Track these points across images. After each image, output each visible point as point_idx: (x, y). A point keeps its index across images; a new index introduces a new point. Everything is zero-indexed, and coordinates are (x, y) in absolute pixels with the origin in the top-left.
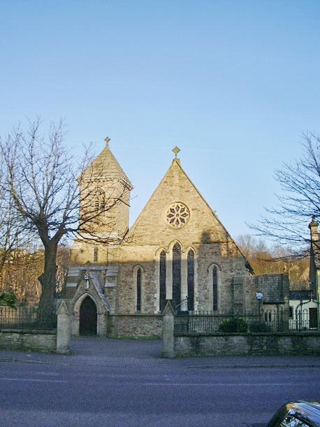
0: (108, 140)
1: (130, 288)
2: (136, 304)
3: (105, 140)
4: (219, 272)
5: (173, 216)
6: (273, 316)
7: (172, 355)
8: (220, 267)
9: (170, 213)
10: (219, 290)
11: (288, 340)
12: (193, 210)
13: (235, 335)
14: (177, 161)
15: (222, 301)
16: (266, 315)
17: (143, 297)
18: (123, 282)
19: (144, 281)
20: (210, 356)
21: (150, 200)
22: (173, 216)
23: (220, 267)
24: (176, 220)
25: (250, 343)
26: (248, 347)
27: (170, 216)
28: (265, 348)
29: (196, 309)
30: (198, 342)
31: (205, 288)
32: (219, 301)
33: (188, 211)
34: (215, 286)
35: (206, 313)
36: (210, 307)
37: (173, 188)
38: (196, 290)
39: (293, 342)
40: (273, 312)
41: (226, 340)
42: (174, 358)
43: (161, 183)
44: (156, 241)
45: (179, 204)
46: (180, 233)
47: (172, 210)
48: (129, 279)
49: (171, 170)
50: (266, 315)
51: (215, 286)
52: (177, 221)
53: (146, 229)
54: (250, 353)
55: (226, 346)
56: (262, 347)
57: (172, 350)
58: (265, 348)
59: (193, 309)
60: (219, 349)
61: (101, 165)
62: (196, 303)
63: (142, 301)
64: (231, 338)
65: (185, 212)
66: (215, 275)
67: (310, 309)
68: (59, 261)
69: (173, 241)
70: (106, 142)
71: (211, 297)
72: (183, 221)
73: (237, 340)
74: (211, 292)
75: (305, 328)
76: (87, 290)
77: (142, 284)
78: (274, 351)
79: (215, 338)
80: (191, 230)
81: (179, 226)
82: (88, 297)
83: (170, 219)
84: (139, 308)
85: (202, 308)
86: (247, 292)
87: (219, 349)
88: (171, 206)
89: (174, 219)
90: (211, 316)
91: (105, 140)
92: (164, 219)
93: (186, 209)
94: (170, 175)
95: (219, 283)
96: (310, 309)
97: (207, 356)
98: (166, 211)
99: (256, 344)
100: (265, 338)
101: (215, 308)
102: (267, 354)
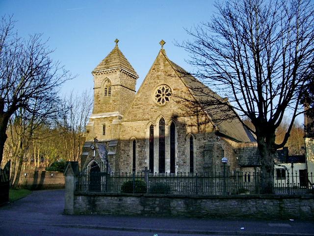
0: (117, 41)
1: (128, 156)
2: (132, 168)
3: (115, 42)
4: (194, 140)
5: (160, 96)
6: (252, 177)
7: (72, 212)
8: (195, 136)
9: (158, 93)
10: (195, 155)
11: (181, 202)
12: (174, 90)
13: (128, 196)
14: (163, 51)
15: (197, 165)
16: (245, 176)
17: (137, 163)
18: (123, 150)
19: (137, 149)
20: (105, 215)
21: (143, 84)
22: (160, 96)
23: (195, 136)
24: (162, 99)
25: (143, 204)
26: (141, 208)
27: (158, 96)
28: (157, 209)
29: (176, 171)
30: (94, 201)
31: (183, 154)
32: (195, 165)
33: (171, 91)
34: (192, 153)
35: (183, 175)
36: (188, 170)
37: (159, 73)
38: (176, 156)
39: (185, 203)
40: (251, 174)
41: (120, 200)
42: (74, 215)
43: (150, 71)
44: (146, 117)
45: (164, 86)
46: (165, 110)
47: (159, 91)
48: (127, 148)
49: (158, 60)
50: (245, 176)
51: (192, 153)
52: (163, 100)
53: (139, 108)
54: (142, 214)
55: (119, 206)
56: (154, 208)
57: (72, 207)
58: (157, 209)
59: (174, 172)
60: (113, 209)
61: (52, 60)
62: (177, 167)
63: (136, 165)
64: (124, 199)
65: (169, 92)
66: (191, 143)
67: (300, 170)
68: (293, 126)
69: (159, 116)
70: (115, 43)
71: (188, 161)
72: (167, 99)
73: (130, 201)
74: (189, 157)
75: (295, 188)
76: (94, 157)
77: (137, 152)
78: (167, 213)
79: (110, 198)
80: (172, 106)
81: (164, 104)
82: (94, 163)
83: (158, 99)
84: (134, 170)
85: (181, 171)
86: (218, 156)
87: (113, 209)
88: (158, 88)
89: (160, 99)
90: (189, 177)
91: (115, 42)
92: (154, 99)
93: (169, 90)
94: (157, 63)
95: (195, 150)
96: (300, 170)
97: (102, 215)
98: (155, 92)
99: (149, 205)
100: (158, 199)
101: (192, 170)
102: (158, 215)
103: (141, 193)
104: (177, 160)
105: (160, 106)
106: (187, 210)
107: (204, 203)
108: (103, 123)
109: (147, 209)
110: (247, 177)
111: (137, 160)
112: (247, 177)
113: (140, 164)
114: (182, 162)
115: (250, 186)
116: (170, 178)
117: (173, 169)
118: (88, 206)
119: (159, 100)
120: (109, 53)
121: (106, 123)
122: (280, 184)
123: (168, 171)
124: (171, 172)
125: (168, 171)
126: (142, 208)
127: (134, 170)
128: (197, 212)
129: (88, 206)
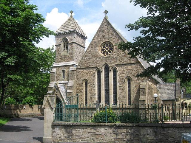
70: (70, 14)
84: (86, 103)
95: (132, 88)
103: (114, 122)
104: (118, 96)
105: (105, 57)
106: (155, 137)
107: (170, 131)
108: (63, 70)
109: (120, 137)
110: (167, 108)
111: (88, 96)
112: (167, 108)
113: (91, 98)
114: (122, 98)
115: (186, 116)
116: (114, 109)
117: (115, 102)
118: (65, 135)
119: (107, 54)
120: (66, 20)
121: (65, 70)
122: (160, 113)
123: (112, 102)
124: (114, 104)
125: (112, 102)
126: (114, 136)
127: (86, 103)
128: (166, 139)
129: (65, 135)
